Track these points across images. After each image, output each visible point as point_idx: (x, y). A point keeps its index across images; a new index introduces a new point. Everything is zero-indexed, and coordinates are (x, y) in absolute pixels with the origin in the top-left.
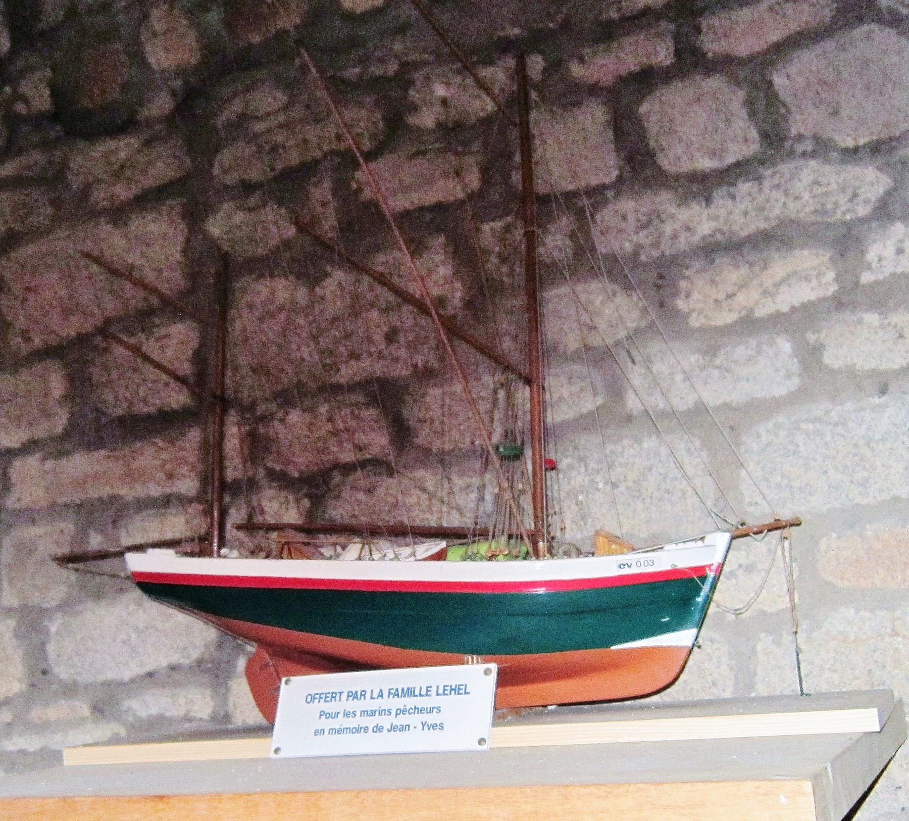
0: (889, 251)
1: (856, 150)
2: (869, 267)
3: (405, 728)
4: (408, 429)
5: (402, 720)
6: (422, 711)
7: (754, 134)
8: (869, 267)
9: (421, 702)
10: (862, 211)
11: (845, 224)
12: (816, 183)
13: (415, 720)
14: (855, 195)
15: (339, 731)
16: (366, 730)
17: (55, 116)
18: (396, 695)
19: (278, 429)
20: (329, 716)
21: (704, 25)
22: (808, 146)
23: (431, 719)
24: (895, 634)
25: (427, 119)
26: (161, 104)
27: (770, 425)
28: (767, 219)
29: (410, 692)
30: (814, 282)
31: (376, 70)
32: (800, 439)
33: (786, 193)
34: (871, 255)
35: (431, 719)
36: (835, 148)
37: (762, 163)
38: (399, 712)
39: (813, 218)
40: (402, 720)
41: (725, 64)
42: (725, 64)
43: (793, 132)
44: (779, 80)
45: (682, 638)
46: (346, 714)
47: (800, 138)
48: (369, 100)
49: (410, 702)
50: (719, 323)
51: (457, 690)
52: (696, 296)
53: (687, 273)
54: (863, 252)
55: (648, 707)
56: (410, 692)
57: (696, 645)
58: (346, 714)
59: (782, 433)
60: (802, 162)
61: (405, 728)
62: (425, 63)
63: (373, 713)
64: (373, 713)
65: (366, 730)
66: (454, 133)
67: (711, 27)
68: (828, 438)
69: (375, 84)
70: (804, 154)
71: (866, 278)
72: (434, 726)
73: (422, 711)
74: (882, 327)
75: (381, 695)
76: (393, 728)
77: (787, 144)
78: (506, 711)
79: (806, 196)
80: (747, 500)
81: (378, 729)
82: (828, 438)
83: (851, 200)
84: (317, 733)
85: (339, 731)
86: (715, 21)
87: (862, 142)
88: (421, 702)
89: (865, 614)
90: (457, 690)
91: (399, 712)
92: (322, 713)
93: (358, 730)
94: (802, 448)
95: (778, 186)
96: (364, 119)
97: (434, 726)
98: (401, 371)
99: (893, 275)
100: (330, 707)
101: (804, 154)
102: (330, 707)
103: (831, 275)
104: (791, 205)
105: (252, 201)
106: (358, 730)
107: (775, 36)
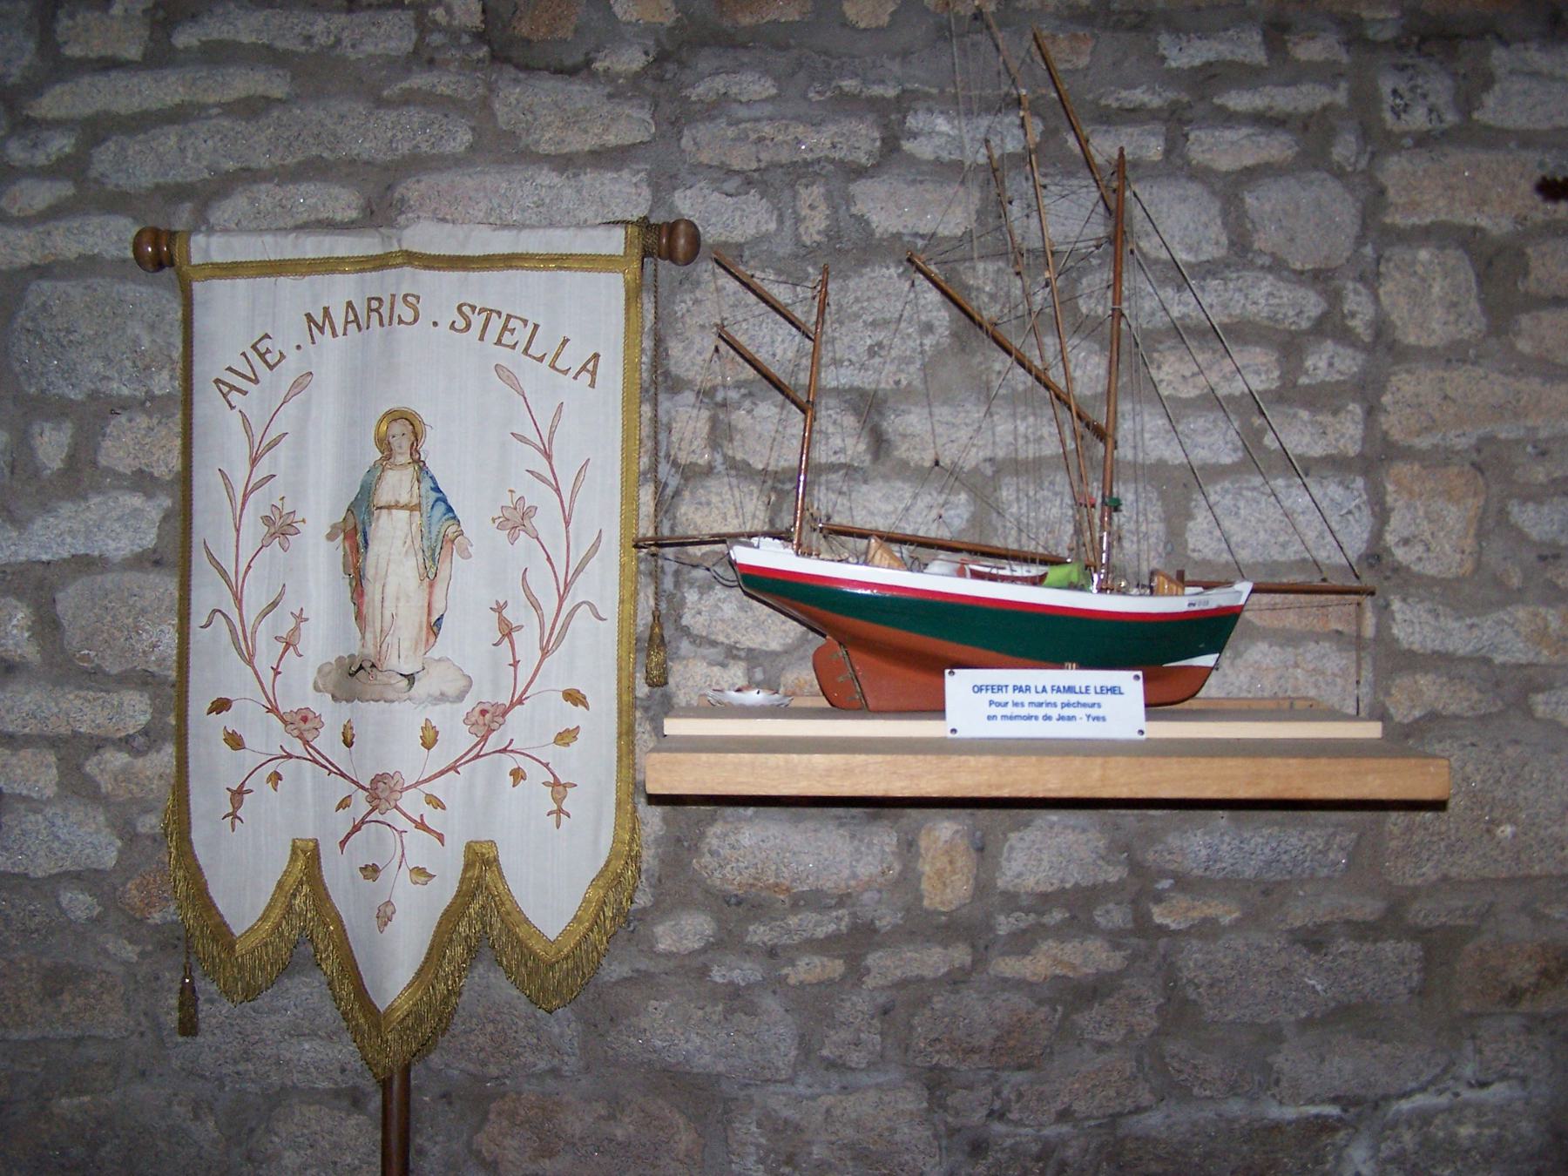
0: (1322, 364)
1: (1302, 273)
2: (1306, 373)
3: (1071, 718)
4: (888, 441)
5: (1067, 712)
6: (1084, 705)
7: (1224, 240)
8: (1306, 373)
9: (1083, 698)
10: (1305, 325)
11: (1290, 332)
12: (1271, 294)
13: (1080, 712)
14: (1301, 312)
15: (1011, 718)
16: (1036, 718)
17: (480, 37)
18: (1059, 690)
19: (740, 418)
20: (999, 705)
21: (1192, 136)
22: (1267, 261)
23: (1095, 712)
24: (1296, 666)
25: (922, 149)
26: (630, 60)
27: (1218, 488)
28: (1230, 315)
29: (1070, 690)
30: (1263, 377)
31: (877, 90)
32: (1242, 504)
33: (1246, 296)
34: (1309, 363)
35: (1095, 712)
36: (1287, 268)
37: (1227, 266)
38: (1065, 705)
39: (1266, 322)
40: (1067, 712)
41: (1201, 175)
42: (1201, 175)
43: (1256, 246)
44: (1249, 200)
45: (1207, 660)
46: (1016, 704)
47: (1261, 252)
48: (871, 117)
49: (1073, 698)
50: (1184, 395)
51: (1113, 690)
52: (1165, 368)
53: (1161, 347)
54: (1302, 361)
55: (1173, 712)
56: (1070, 690)
57: (1216, 667)
58: (1016, 704)
59: (1229, 497)
60: (1261, 275)
61: (1071, 718)
62: (928, 96)
63: (1040, 705)
64: (1040, 705)
65: (1036, 718)
66: (949, 170)
67: (1198, 139)
68: (1263, 505)
69: (877, 106)
70: (1262, 267)
71: (1303, 380)
72: (1097, 718)
73: (1084, 705)
74: (1312, 423)
75: (1044, 690)
76: (1061, 718)
77: (1250, 256)
78: (1155, 707)
79: (1262, 301)
80: (1191, 546)
81: (1047, 718)
82: (1263, 505)
83: (1297, 315)
84: (989, 718)
85: (1011, 718)
86: (1202, 134)
87: (1308, 267)
88: (1083, 698)
89: (1276, 649)
90: (1113, 690)
91: (1065, 705)
92: (991, 703)
93: (1029, 718)
94: (1242, 512)
95: (1240, 290)
96: (863, 138)
97: (1097, 718)
98: (886, 385)
99: (1323, 382)
100: (999, 697)
101: (1262, 267)
102: (999, 697)
103: (1276, 374)
104: (1249, 307)
105: (731, 185)
106: (1029, 718)
107: (1249, 161)
